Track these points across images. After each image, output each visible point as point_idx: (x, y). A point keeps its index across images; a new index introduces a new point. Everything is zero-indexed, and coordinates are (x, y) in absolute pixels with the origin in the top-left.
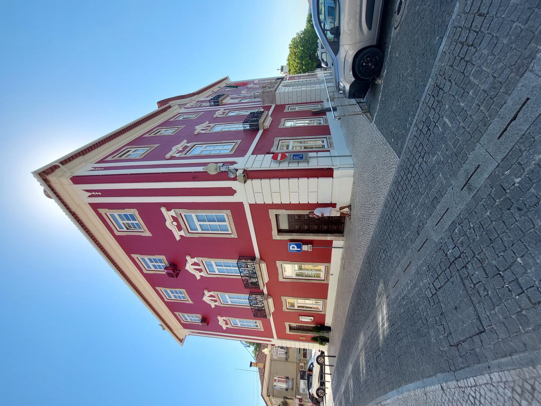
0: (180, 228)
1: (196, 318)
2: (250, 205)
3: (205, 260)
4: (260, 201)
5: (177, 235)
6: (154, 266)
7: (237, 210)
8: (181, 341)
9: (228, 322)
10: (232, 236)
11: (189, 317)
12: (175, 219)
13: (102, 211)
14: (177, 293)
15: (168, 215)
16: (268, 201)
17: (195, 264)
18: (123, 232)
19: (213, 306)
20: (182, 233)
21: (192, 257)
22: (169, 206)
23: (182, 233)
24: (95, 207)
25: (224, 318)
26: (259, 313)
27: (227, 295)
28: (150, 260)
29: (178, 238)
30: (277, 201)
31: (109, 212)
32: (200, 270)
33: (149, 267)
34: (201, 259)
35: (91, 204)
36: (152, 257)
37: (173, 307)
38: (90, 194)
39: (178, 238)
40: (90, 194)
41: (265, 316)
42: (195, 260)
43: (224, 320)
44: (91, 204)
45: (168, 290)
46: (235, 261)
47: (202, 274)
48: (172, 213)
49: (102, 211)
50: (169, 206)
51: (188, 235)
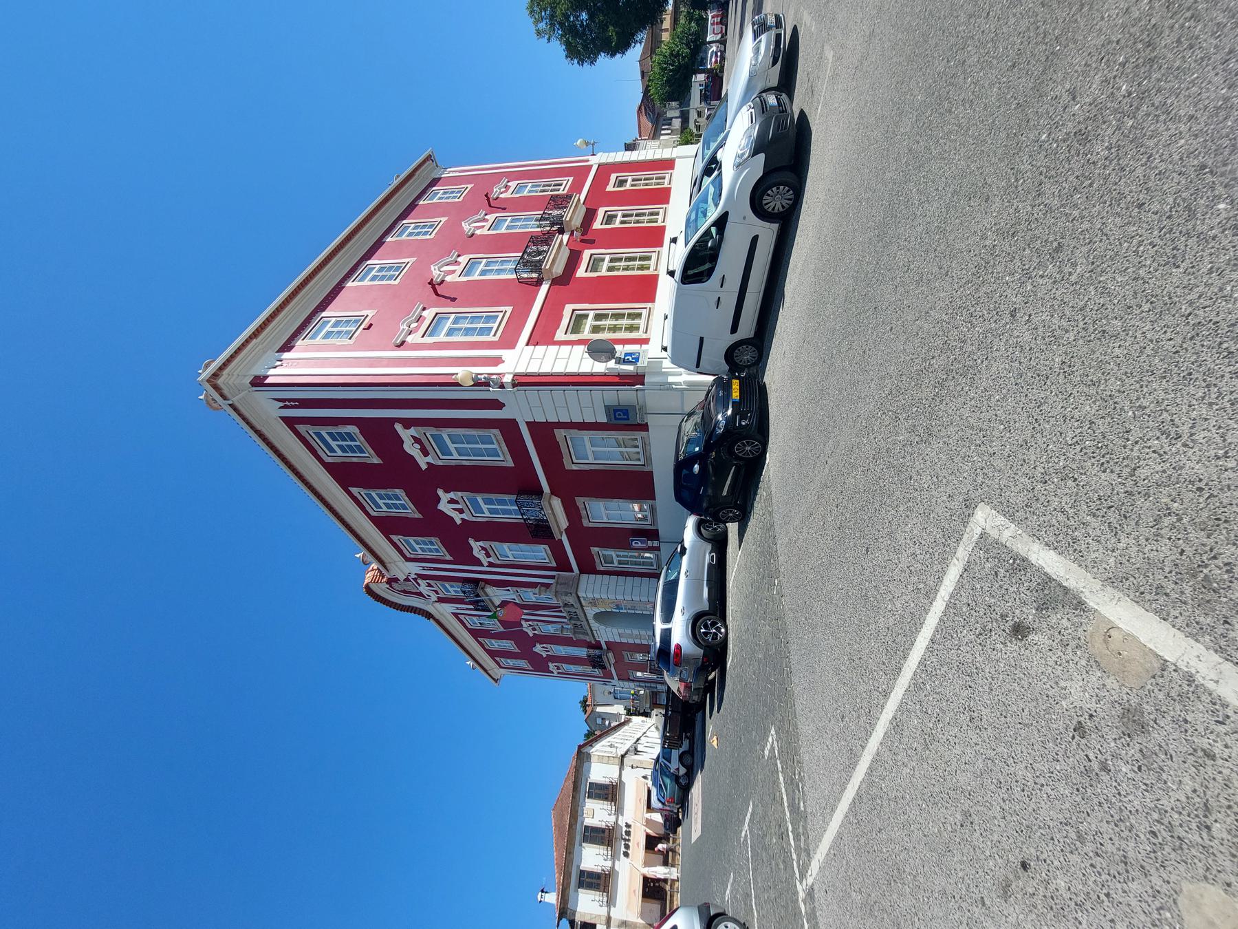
0: (425, 453)
1: (508, 645)
2: (527, 423)
3: (466, 495)
4: (540, 419)
5: (423, 461)
6: (387, 506)
7: (509, 429)
8: (496, 681)
9: (491, 553)
10: (503, 464)
11: (418, 543)
12: (417, 440)
13: (301, 428)
14: (390, 498)
15: (406, 435)
16: (552, 419)
17: (452, 501)
18: (338, 456)
19: (459, 522)
20: (429, 459)
21: (447, 491)
22: (408, 423)
23: (429, 459)
24: (290, 422)
25: (481, 543)
26: (539, 532)
27: (505, 547)
28: (330, 434)
29: (424, 467)
30: (565, 419)
31: (312, 430)
32: (461, 511)
33: (332, 450)
34: (460, 494)
35: (284, 419)
36: (383, 492)
37: (388, 526)
38: (282, 404)
39: (424, 467)
40: (282, 404)
41: (551, 536)
42: (452, 495)
43: (483, 548)
44: (284, 419)
45: (411, 540)
46: (514, 497)
47: (464, 516)
48: (412, 431)
49: (462, 617)
50: (408, 423)
51: (440, 463)
